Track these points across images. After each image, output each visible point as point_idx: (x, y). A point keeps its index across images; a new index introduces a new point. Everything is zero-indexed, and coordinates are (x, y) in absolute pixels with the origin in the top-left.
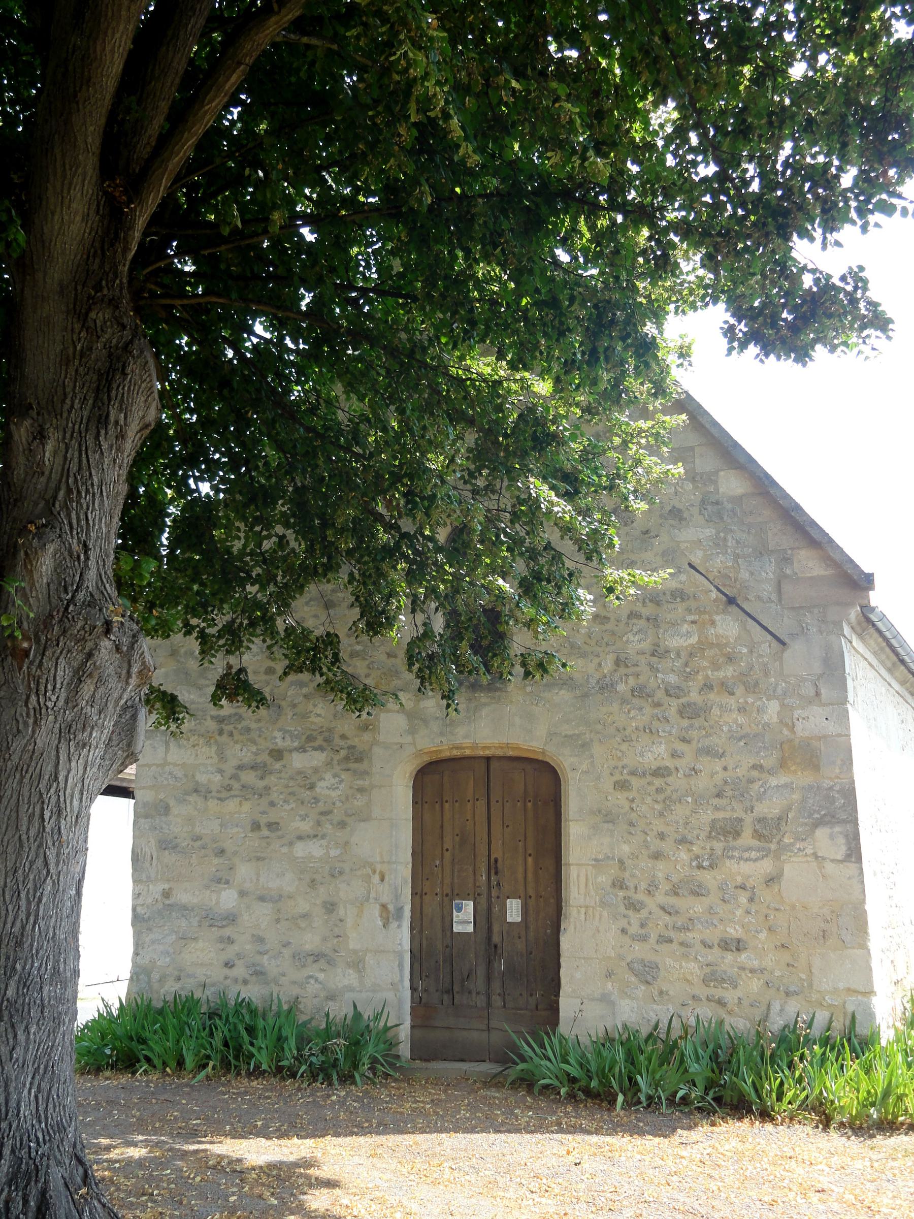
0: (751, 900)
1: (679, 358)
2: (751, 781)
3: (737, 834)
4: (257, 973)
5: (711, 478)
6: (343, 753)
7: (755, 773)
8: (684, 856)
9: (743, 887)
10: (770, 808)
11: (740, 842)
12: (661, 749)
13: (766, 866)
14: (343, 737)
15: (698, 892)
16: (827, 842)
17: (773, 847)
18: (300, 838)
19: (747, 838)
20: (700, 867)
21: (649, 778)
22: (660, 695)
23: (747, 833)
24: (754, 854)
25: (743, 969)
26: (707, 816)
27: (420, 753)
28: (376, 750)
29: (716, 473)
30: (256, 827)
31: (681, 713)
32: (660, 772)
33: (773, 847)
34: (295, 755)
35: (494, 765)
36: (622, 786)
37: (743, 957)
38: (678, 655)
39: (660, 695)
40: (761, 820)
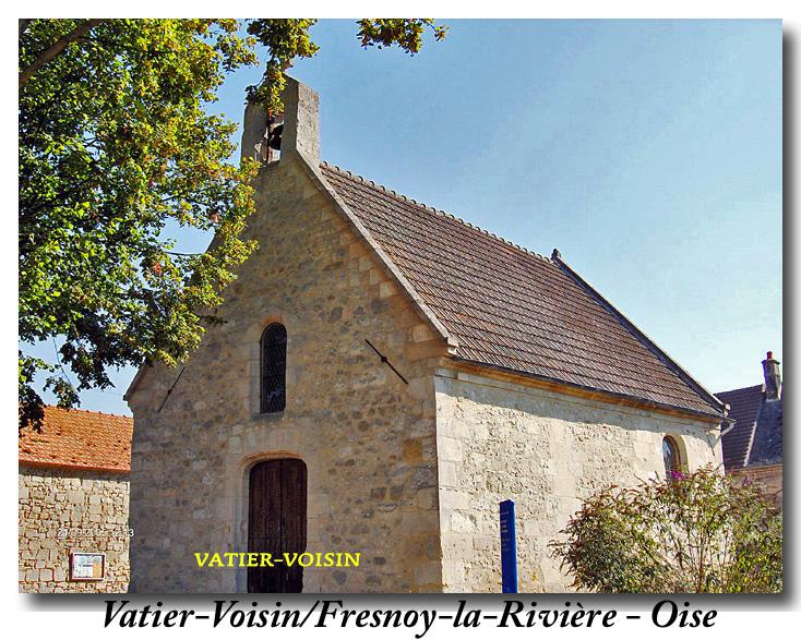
0: (388, 534)
1: (343, 413)
2: (391, 465)
3: (383, 496)
4: (178, 583)
5: (377, 288)
6: (214, 461)
7: (392, 461)
8: (357, 511)
9: (230, 355)
10: (397, 481)
11: (384, 501)
12: (349, 449)
13: (396, 514)
14: (214, 452)
15: (366, 531)
16: (424, 498)
17: (399, 503)
18: (196, 509)
19: (388, 499)
20: (365, 516)
21: (344, 467)
22: (350, 418)
23: (388, 495)
24: (391, 508)
25: (384, 574)
26: (369, 488)
27: (246, 459)
28: (227, 458)
29: (379, 285)
30: (178, 503)
31: (360, 427)
32: (351, 462)
33: (399, 503)
34: (195, 463)
35: (433, 490)
36: (332, 472)
37: (384, 568)
38: (359, 393)
39: (350, 418)
40: (393, 488)
